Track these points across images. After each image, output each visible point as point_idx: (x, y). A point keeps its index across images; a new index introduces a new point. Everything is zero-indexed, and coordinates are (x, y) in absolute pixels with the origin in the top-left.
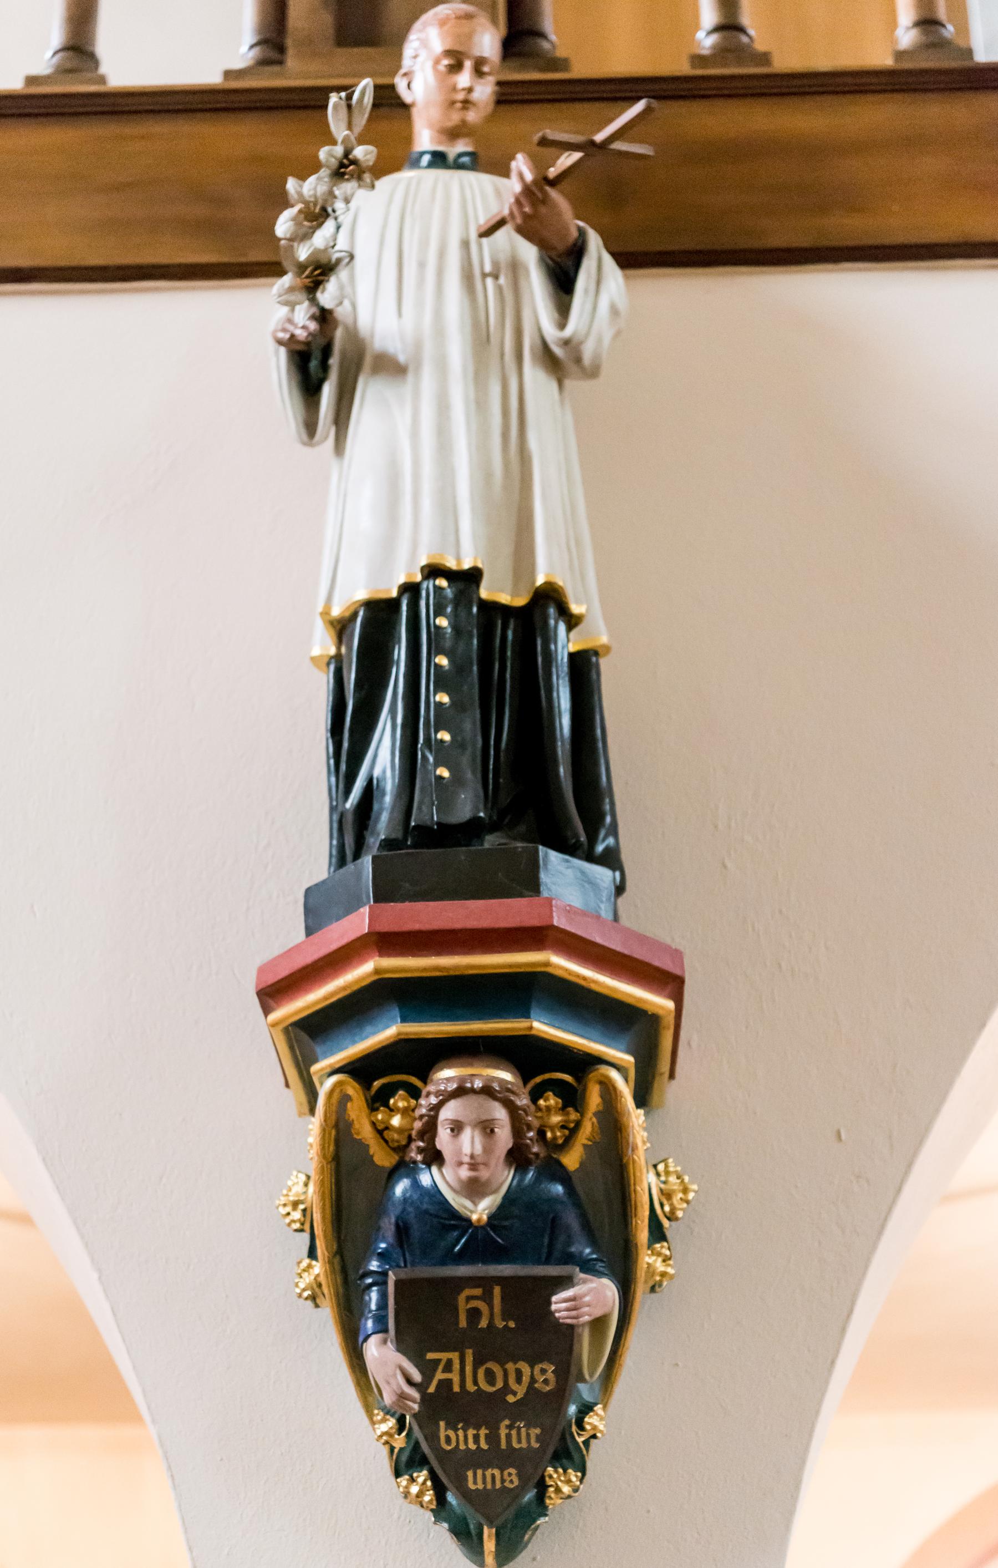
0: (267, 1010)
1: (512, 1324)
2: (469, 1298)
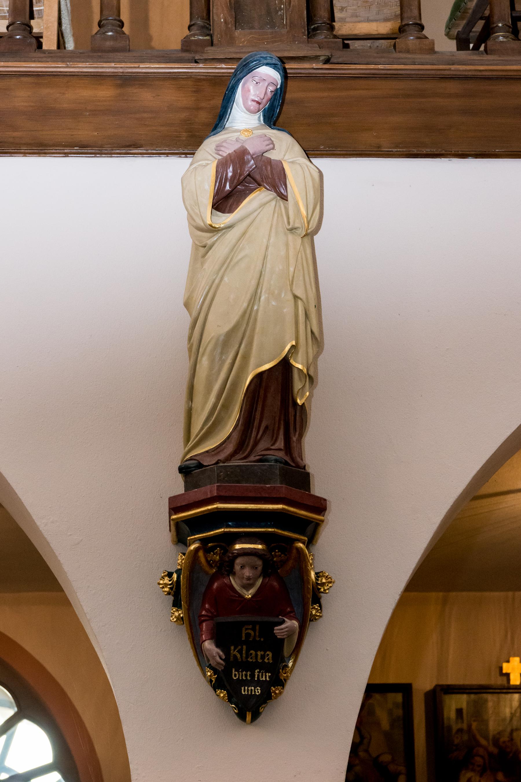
2: (246, 629)
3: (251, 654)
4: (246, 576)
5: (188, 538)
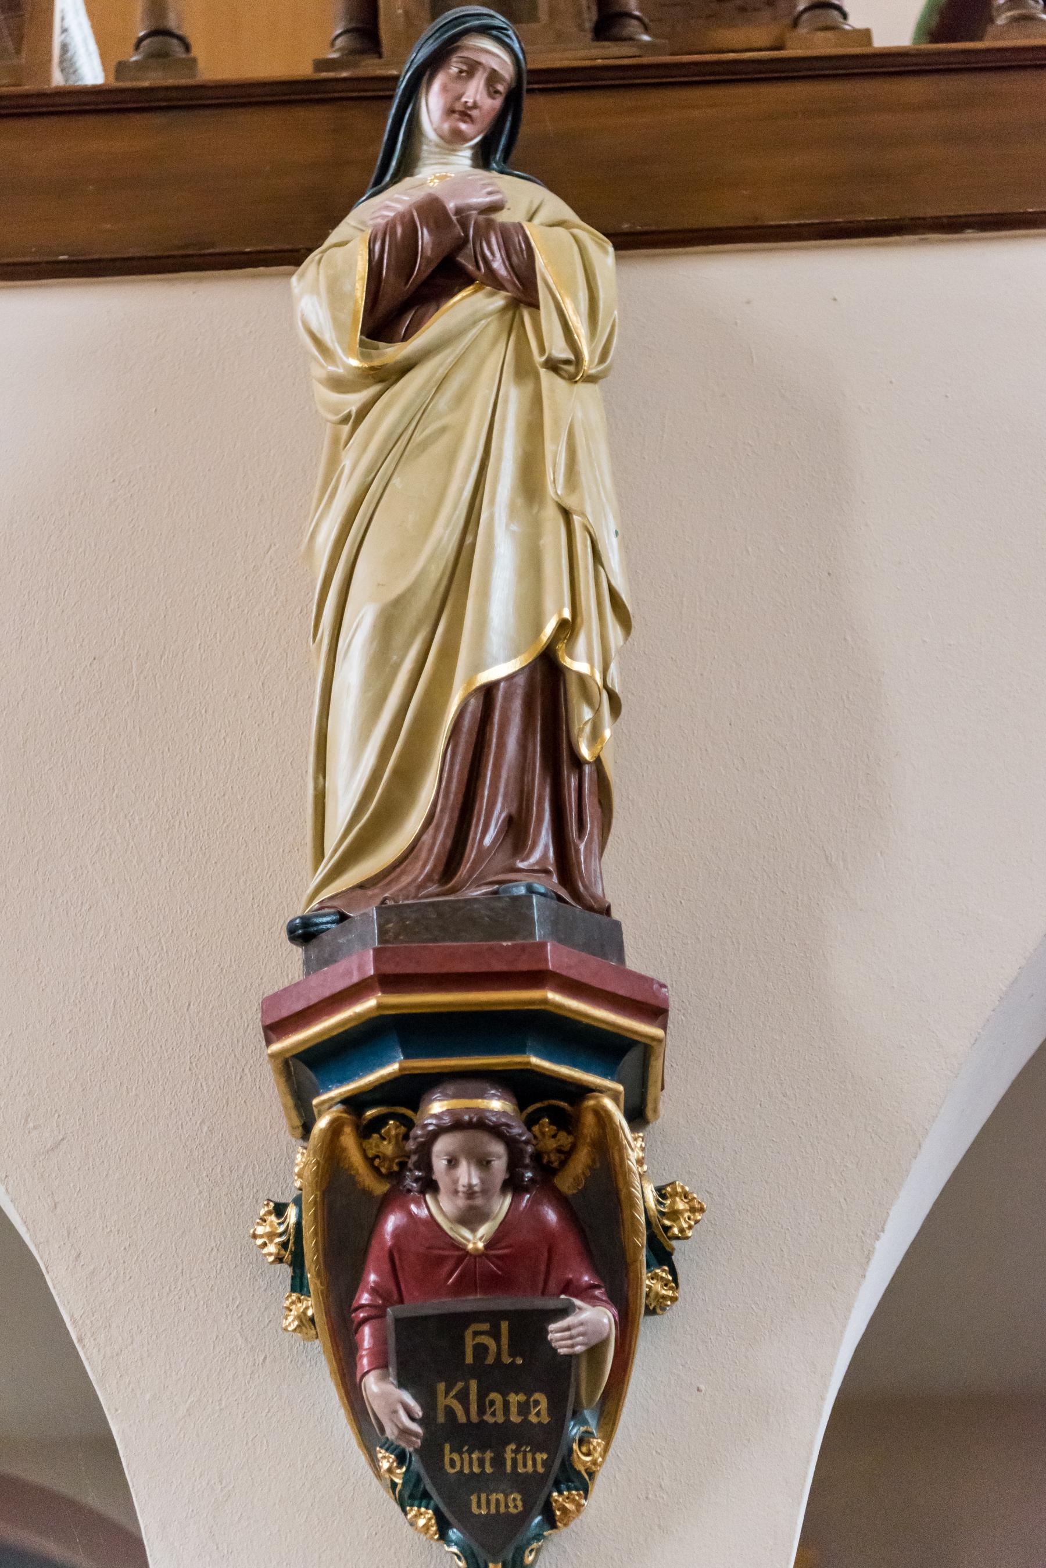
0: (269, 1042)
1: (519, 1361)
2: (476, 1334)
3: (492, 1403)
4: (464, 1186)
5: (315, 1102)
